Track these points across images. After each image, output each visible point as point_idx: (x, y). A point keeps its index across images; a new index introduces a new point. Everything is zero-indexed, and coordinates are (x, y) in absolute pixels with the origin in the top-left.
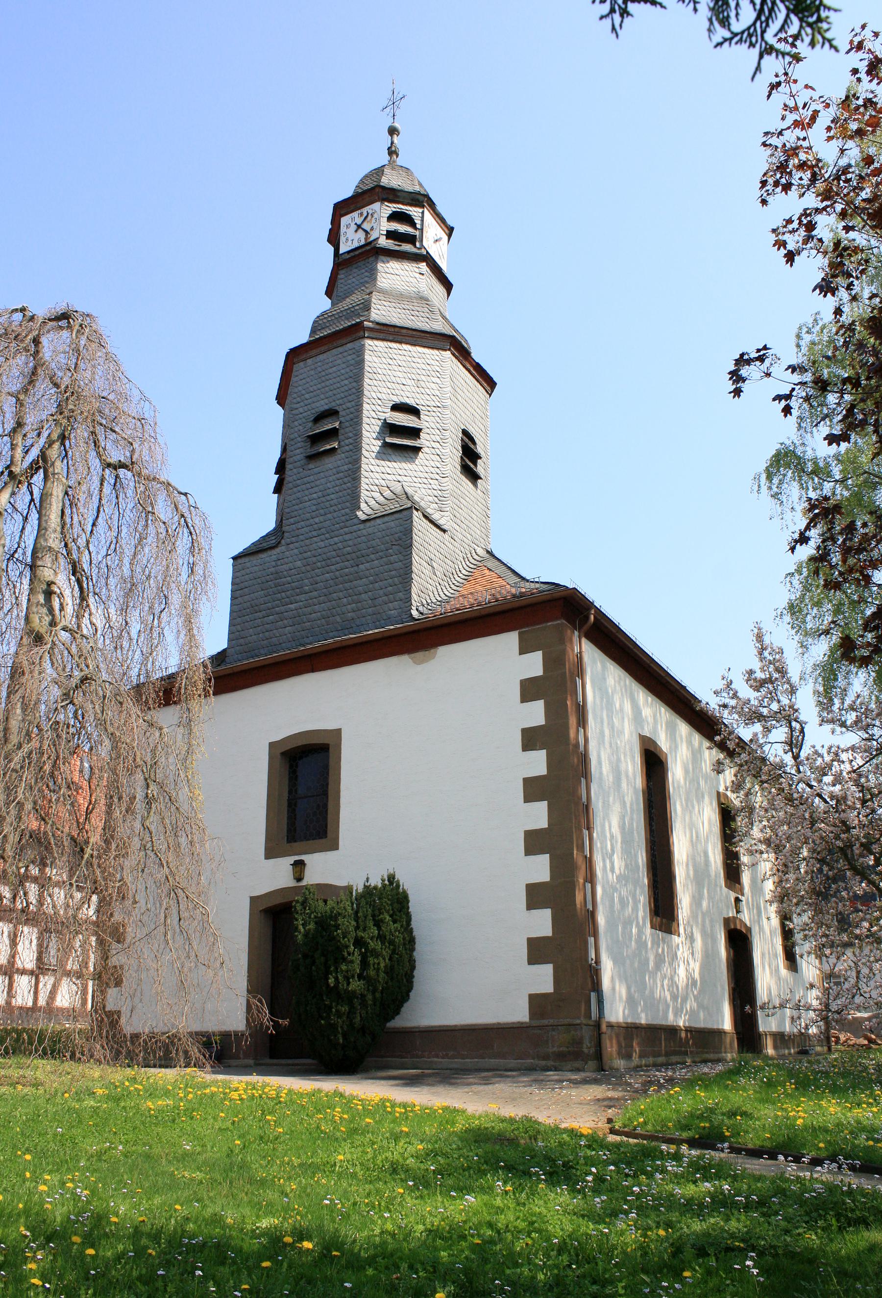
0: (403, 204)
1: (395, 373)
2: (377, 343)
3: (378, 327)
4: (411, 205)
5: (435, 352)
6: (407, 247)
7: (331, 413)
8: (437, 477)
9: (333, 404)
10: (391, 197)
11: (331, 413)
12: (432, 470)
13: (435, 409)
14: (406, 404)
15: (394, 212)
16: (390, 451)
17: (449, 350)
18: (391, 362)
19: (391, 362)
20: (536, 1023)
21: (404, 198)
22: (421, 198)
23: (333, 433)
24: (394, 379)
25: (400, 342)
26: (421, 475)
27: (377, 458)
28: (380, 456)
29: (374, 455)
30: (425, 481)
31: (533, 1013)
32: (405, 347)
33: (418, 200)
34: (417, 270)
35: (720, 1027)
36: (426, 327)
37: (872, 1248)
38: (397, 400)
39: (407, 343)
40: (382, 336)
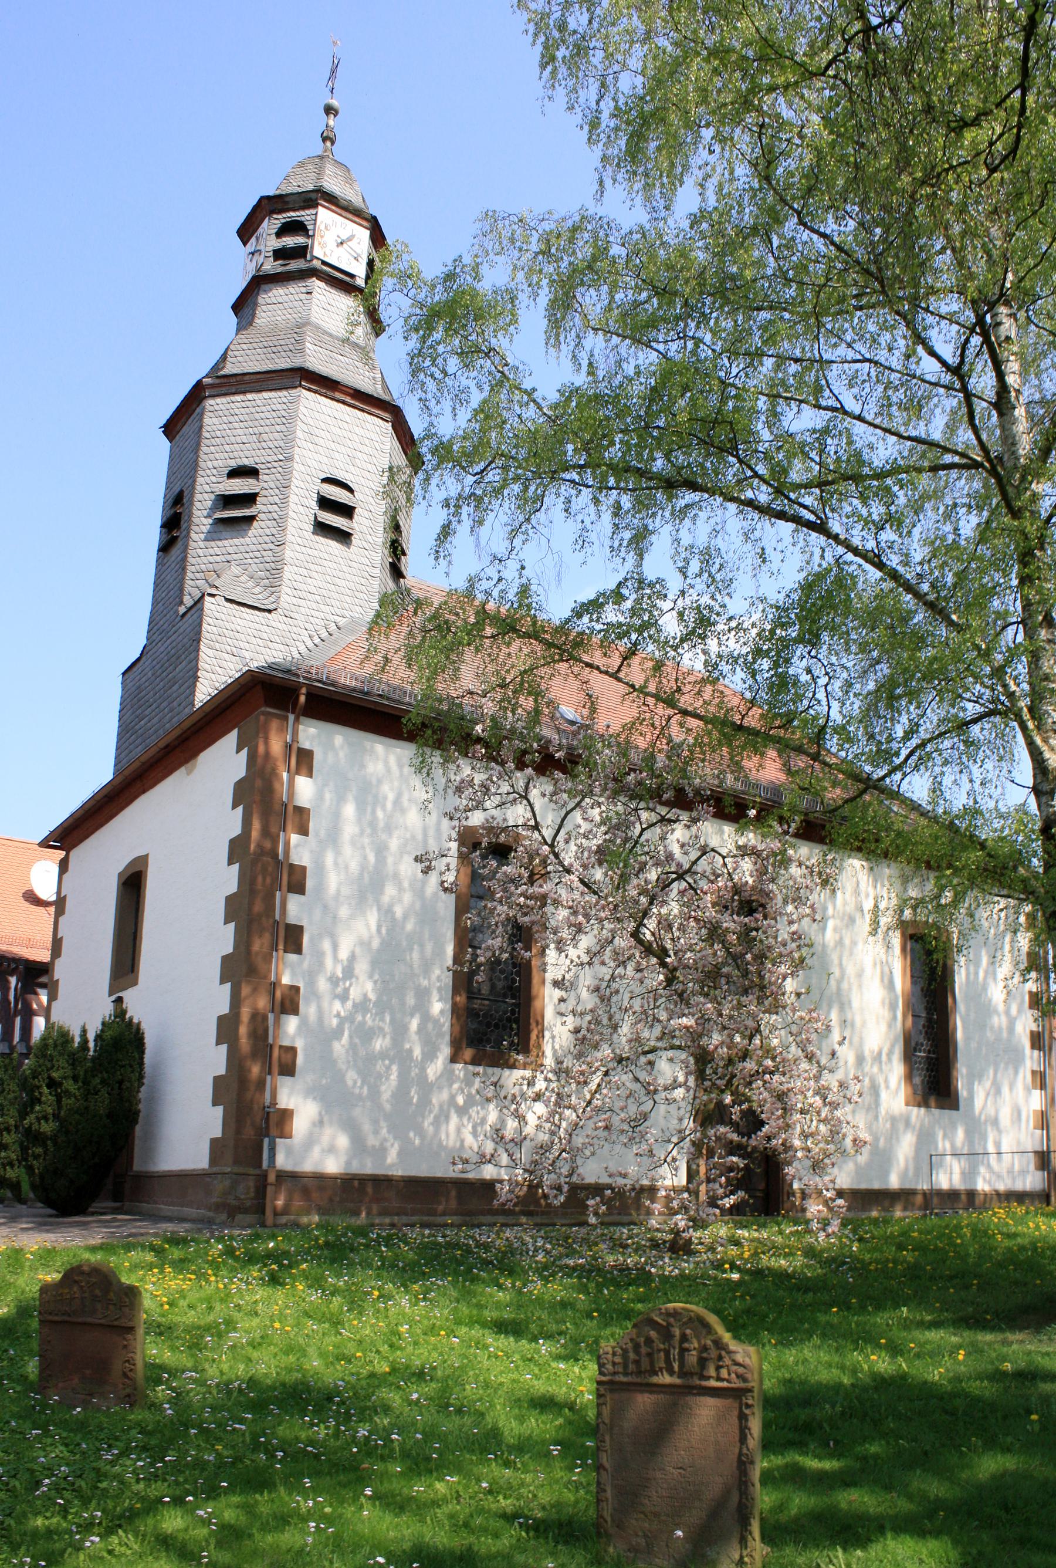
0: (294, 210)
1: (235, 432)
2: (219, 400)
3: (218, 381)
4: (303, 208)
5: (285, 393)
6: (296, 265)
7: (250, 472)
8: (271, 546)
9: (257, 460)
10: (279, 206)
11: (250, 472)
12: (267, 539)
13: (276, 464)
14: (245, 466)
15: (284, 224)
16: (221, 527)
17: (300, 385)
18: (231, 419)
19: (231, 419)
20: (215, 1169)
21: (295, 202)
22: (313, 196)
23: (250, 499)
24: (233, 439)
25: (244, 393)
26: (254, 548)
27: (206, 540)
28: (211, 537)
29: (202, 536)
30: (258, 554)
31: (214, 1159)
32: (250, 396)
33: (311, 200)
34: (304, 290)
35: (143, 1169)
36: (271, 367)
37: (1028, 1376)
38: (233, 464)
39: (251, 392)
40: (224, 390)
